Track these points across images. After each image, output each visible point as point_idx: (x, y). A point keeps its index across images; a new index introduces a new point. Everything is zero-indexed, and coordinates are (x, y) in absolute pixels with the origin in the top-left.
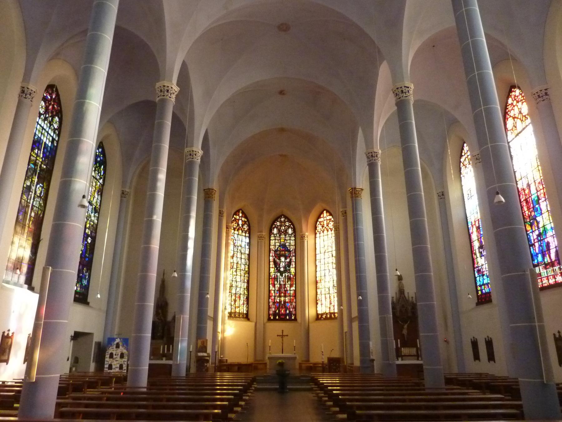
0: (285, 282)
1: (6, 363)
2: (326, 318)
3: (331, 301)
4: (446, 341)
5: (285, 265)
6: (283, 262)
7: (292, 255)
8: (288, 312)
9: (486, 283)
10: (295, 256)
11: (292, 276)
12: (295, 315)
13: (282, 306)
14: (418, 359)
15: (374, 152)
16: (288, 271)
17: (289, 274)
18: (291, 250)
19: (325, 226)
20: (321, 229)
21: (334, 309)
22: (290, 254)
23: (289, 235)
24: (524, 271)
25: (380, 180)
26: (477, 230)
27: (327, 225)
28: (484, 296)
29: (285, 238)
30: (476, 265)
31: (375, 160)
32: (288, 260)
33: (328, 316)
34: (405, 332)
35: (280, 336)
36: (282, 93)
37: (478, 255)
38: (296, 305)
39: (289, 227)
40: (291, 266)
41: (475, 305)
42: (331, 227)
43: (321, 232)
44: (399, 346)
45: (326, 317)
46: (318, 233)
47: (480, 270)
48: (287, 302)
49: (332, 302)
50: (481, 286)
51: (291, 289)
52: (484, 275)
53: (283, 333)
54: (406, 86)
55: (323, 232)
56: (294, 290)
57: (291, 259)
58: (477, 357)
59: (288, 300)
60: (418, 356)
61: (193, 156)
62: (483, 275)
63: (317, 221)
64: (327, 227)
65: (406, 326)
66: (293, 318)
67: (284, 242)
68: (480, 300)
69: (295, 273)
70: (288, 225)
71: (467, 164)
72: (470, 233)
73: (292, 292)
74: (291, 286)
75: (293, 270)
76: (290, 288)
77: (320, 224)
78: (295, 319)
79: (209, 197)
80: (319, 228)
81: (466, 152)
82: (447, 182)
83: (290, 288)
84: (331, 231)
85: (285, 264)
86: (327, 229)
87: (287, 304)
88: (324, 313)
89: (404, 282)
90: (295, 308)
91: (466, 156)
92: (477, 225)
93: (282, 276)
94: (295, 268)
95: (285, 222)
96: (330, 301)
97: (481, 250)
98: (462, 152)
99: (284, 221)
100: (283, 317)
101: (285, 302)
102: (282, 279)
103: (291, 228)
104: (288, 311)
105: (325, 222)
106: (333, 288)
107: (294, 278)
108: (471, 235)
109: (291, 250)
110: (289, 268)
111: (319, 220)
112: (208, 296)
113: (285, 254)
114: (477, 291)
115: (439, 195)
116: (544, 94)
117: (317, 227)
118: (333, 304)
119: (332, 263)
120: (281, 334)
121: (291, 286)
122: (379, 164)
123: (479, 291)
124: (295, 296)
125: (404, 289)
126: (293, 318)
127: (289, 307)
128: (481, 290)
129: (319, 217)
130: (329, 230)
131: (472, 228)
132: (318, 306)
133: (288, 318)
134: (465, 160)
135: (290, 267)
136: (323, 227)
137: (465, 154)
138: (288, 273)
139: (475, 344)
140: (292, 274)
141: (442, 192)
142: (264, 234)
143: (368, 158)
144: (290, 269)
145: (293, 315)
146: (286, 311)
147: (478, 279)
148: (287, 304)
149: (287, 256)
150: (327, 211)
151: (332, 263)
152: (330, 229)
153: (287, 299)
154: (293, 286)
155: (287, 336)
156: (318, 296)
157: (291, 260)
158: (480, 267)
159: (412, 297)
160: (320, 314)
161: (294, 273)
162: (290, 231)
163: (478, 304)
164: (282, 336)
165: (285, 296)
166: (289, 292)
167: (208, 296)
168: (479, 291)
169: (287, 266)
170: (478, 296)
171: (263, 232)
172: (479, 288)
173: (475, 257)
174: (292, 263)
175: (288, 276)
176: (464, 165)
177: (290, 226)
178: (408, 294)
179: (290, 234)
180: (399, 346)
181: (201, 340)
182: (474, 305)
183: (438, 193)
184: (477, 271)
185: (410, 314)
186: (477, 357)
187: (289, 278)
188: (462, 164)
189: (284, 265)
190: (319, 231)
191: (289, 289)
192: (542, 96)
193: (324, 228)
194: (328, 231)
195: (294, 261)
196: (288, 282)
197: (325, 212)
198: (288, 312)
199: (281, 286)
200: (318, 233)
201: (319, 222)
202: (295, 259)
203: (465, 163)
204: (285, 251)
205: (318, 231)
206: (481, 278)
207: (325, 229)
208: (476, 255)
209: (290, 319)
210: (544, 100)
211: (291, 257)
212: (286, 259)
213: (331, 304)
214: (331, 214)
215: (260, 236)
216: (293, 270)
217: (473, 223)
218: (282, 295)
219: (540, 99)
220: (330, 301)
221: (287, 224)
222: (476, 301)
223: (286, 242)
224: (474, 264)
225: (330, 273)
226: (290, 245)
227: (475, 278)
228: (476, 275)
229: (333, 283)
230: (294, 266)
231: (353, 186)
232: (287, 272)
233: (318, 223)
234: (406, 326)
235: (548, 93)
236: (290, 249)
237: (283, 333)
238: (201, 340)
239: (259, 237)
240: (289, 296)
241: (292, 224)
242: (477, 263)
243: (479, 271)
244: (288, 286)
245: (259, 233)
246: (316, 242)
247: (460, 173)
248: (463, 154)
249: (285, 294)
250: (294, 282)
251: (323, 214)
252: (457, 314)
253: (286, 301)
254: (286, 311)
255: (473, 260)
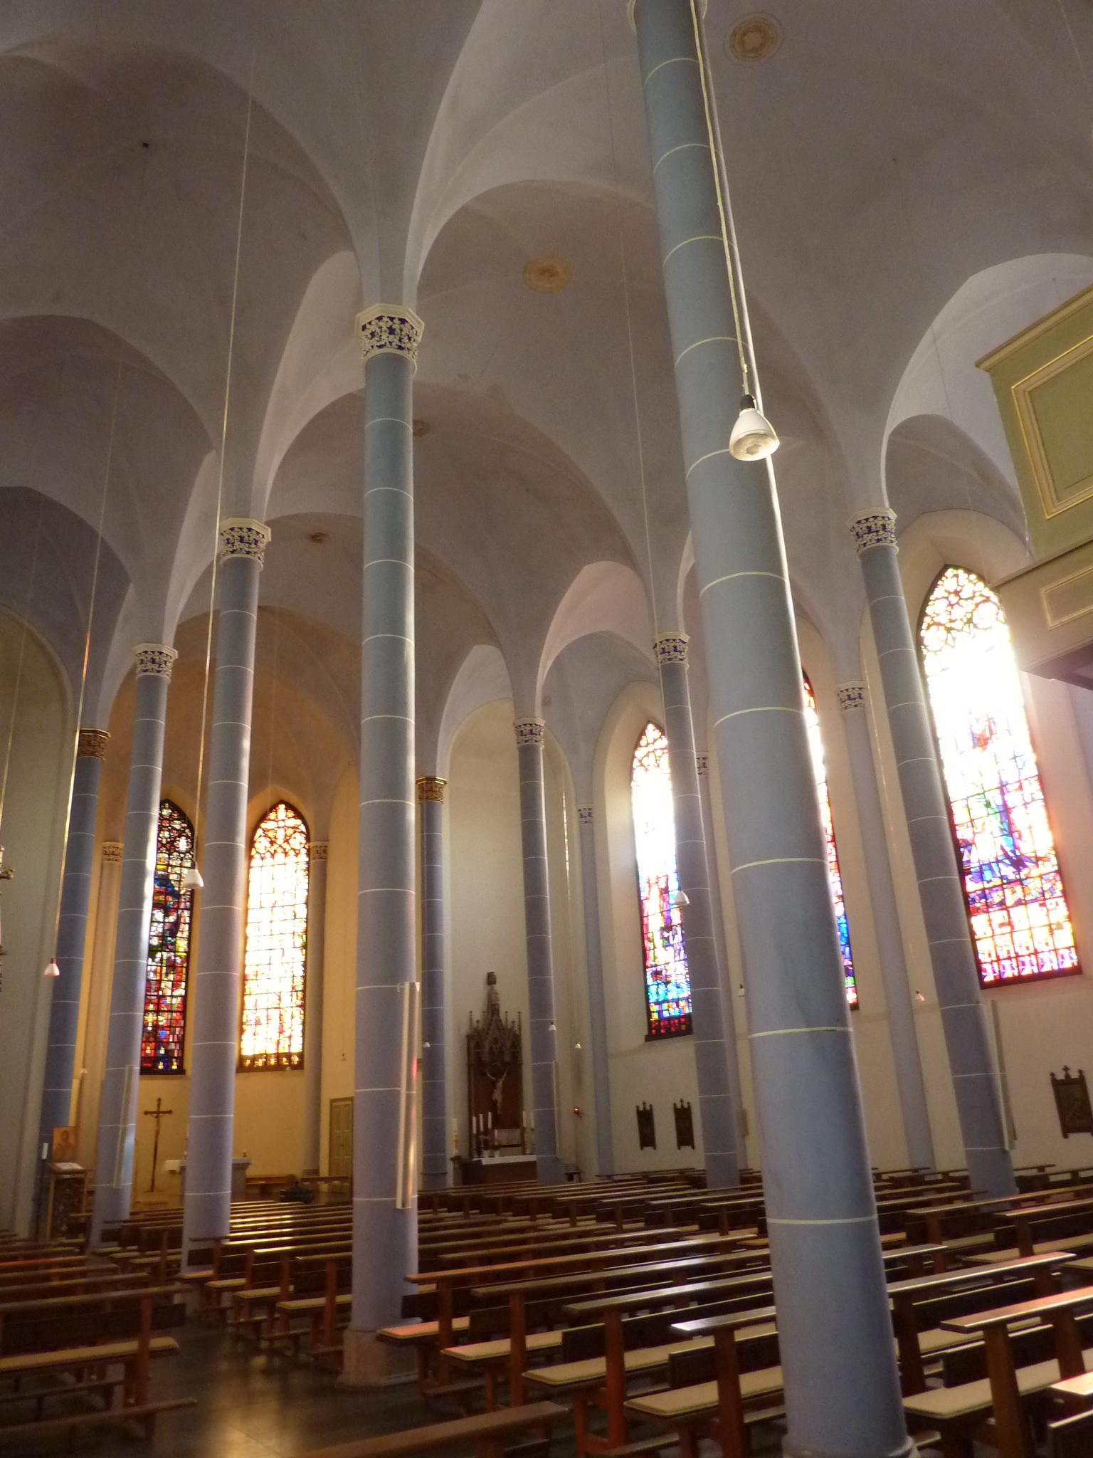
0: (161, 976)
1: (251, 1172)
2: (266, 1068)
3: (283, 1026)
4: (577, 1113)
5: (164, 931)
6: (159, 922)
7: (182, 906)
8: (162, 1051)
9: (673, 999)
10: (191, 909)
11: (179, 960)
12: (181, 1060)
13: (149, 1037)
14: (524, 1154)
15: (537, 725)
16: (170, 947)
17: (172, 954)
18: (182, 892)
19: (280, 841)
20: (266, 847)
21: (290, 1046)
22: (179, 903)
23: (180, 853)
24: (978, 1002)
25: (543, 783)
26: (661, 894)
27: (287, 841)
28: (666, 1022)
29: (168, 862)
30: (650, 962)
31: (536, 741)
32: (172, 919)
33: (273, 1061)
34: (498, 1096)
35: (151, 1113)
36: (316, 538)
37: (659, 942)
38: (183, 1036)
39: (180, 834)
40: (179, 934)
41: (644, 1040)
42: (297, 847)
43: (268, 855)
44: (490, 1126)
45: (265, 1063)
46: (257, 856)
47: (661, 971)
48: (163, 1028)
49: (285, 1028)
50: (658, 1003)
51: (175, 994)
52: (669, 982)
53: (159, 1106)
54: (682, 639)
55: (273, 855)
56: (181, 996)
57: (181, 917)
58: (647, 1139)
59: (165, 1021)
60: (521, 1146)
61: (160, 665)
62: (667, 983)
63: (257, 826)
64: (285, 845)
65: (500, 1084)
66: (174, 1067)
67: (164, 870)
68: (654, 1031)
69: (188, 953)
70: (178, 827)
71: (652, 765)
72: (642, 899)
73: (176, 1001)
74: (175, 985)
75: (182, 945)
76: (173, 991)
77: (266, 836)
78: (181, 1071)
79: (93, 753)
80: (261, 844)
81: (651, 741)
82: (602, 791)
83: (173, 991)
84: (297, 855)
85: (163, 928)
86: (285, 849)
87: (160, 1032)
88: (262, 1055)
89: (498, 987)
90: (181, 1042)
91: (651, 748)
92: (663, 885)
93: (153, 958)
94: (189, 939)
95: (171, 819)
96: (281, 1026)
97: (666, 934)
98: (640, 739)
99: (171, 816)
100: (149, 1065)
101: (156, 1026)
102: (154, 968)
103: (187, 837)
104: (162, 1049)
105: (281, 835)
106: (292, 995)
107: (185, 965)
108: (644, 902)
109: (182, 892)
110: (172, 938)
111: (263, 825)
112: (554, 1028)
113: (166, 901)
114: (649, 1013)
115: (581, 814)
116: (857, 695)
117: (255, 842)
118: (287, 1033)
119: (294, 933)
120: (155, 1109)
121: (175, 985)
122: (542, 748)
123: (654, 1012)
124: (183, 1011)
125: (500, 1003)
126: (174, 1067)
127: (165, 1040)
128: (660, 1012)
129: (264, 818)
130: (292, 853)
131: (647, 889)
132: (243, 1037)
133: (161, 1066)
134: (647, 755)
135: (176, 937)
136: (272, 843)
137: (648, 744)
138: (171, 951)
139: (645, 1118)
140: (179, 954)
141: (590, 809)
142: (121, 845)
143: (522, 733)
144: (175, 942)
145: (174, 1060)
146: (157, 1049)
147: (653, 989)
148: (160, 1032)
149: (170, 908)
150: (289, 807)
151: (294, 933)
152: (294, 850)
153: (163, 1020)
154: (180, 986)
155: (170, 1112)
156: (245, 1012)
157: (179, 917)
158: (662, 967)
159: (513, 1022)
160: (248, 1058)
161: (185, 952)
162: (183, 844)
163: (649, 1038)
164: (158, 1113)
165: (158, 1011)
166: (168, 1000)
167: (554, 1028)
168: (654, 1012)
169: (167, 934)
170: (650, 1023)
171: (118, 842)
172: (654, 1008)
173: (648, 945)
174: (182, 926)
175: (169, 958)
176: (642, 765)
177: (184, 832)
178: (519, 1016)
179: (183, 853)
180: (490, 1126)
181: (62, 1129)
182: (641, 1040)
183: (580, 810)
184: (652, 974)
185: (507, 1058)
186: (647, 1139)
187: (172, 966)
188: (636, 763)
189: (161, 930)
190: (262, 851)
191: (168, 992)
192: (855, 699)
193: (275, 846)
194: (286, 854)
195: (188, 920)
196: (167, 974)
197: (282, 807)
198: (162, 1051)
199: (150, 984)
200: (257, 856)
201: (263, 829)
202: (191, 917)
203: (645, 762)
204: (166, 894)
205: (257, 852)
206: (662, 987)
207: (280, 850)
208: (653, 941)
209: (167, 1071)
210: (856, 706)
211: (180, 911)
212: (166, 915)
213: (281, 1032)
214: (298, 815)
215: (111, 850)
216: (182, 945)
217: (653, 881)
218: (151, 1007)
219: (850, 702)
220: (281, 1026)
221: (177, 825)
222: (646, 1033)
223: (169, 871)
224: (645, 958)
225: (286, 959)
226: (180, 881)
227: (647, 987)
228: (650, 981)
229: (293, 982)
230: (186, 934)
231: (429, 774)
232: (168, 948)
233: (259, 832)
234: (500, 1084)
235: (863, 696)
236: (180, 890)
237: (159, 1106)
238: (62, 1129)
239: (105, 853)
240: (167, 1011)
241: (191, 827)
242: (655, 958)
243: (657, 974)
244: (166, 985)
245: (108, 844)
246: (250, 879)
247: (631, 779)
248: (643, 743)
249: (158, 1005)
250: (184, 976)
251: (276, 812)
252: (603, 1056)
253: (160, 1023)
254: (157, 1049)
255: (644, 952)
